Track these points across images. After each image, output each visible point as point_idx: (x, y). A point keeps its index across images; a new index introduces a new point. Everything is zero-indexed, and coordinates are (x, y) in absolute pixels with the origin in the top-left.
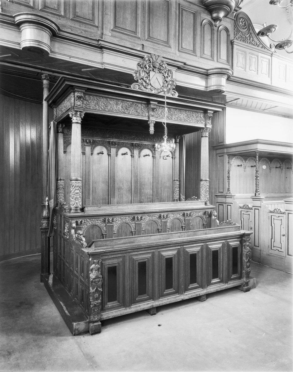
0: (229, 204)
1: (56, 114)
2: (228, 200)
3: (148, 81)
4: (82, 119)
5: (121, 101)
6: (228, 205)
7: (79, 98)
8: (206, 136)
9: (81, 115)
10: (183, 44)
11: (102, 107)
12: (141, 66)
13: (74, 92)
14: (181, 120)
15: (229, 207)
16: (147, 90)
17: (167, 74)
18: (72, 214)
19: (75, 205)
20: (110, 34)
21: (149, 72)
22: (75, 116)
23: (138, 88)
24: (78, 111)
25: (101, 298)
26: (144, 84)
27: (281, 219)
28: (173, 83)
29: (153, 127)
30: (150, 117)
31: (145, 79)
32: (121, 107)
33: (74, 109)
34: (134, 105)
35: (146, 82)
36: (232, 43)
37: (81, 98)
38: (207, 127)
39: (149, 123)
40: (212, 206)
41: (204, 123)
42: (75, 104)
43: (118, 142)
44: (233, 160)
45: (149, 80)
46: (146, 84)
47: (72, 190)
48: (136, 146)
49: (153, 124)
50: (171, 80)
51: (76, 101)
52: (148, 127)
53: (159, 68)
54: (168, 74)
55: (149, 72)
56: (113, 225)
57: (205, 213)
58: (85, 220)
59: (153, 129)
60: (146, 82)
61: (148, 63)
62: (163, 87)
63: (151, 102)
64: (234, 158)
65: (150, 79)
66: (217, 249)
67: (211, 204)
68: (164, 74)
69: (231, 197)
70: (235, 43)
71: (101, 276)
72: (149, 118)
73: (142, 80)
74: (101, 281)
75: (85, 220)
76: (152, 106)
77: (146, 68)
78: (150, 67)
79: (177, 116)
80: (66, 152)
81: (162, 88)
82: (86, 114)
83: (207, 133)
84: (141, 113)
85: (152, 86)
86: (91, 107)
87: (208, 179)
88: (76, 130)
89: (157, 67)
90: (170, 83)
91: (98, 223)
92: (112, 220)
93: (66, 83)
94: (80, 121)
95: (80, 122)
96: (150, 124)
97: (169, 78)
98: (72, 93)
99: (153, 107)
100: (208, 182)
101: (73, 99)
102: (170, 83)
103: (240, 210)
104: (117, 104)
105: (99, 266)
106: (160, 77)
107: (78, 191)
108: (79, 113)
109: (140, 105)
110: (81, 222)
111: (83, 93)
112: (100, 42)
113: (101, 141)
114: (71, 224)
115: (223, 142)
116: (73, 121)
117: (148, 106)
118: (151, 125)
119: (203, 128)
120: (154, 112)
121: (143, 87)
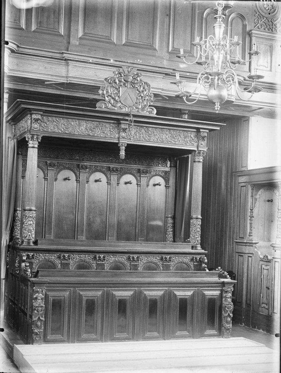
0: (250, 255)
1: (15, 132)
2: (246, 249)
3: (117, 98)
4: (39, 143)
5: (84, 121)
6: (249, 256)
7: (37, 120)
8: (199, 162)
9: (37, 138)
10: (175, 44)
11: (62, 130)
12: (109, 81)
13: (31, 114)
14: (162, 142)
15: (250, 259)
16: (116, 109)
17: (142, 88)
18: (25, 245)
19: (27, 237)
20: (78, 43)
21: (119, 87)
22: (31, 140)
23: (104, 107)
24: (34, 135)
25: (43, 328)
26: (112, 101)
27: (268, 269)
28: (150, 98)
29: (124, 151)
30: (120, 139)
31: (113, 96)
32: (84, 128)
33: (30, 132)
34: (101, 125)
35: (114, 99)
36: (250, 34)
37: (38, 120)
38: (200, 149)
39: (119, 145)
40: (203, 251)
41: (196, 144)
42: (31, 127)
43: (90, 165)
44: (260, 193)
45: (119, 96)
46: (114, 102)
47: (24, 221)
48: (114, 171)
49: (124, 147)
50: (147, 94)
51: (32, 124)
52: (119, 150)
53: (133, 81)
54: (143, 88)
55: (119, 87)
56: (69, 262)
57: (192, 260)
58: (38, 254)
59: (124, 153)
60: (114, 99)
61: (118, 78)
62: (137, 104)
63: (121, 122)
64: (261, 190)
65: (120, 96)
66: (186, 297)
67: (203, 249)
68: (139, 88)
69: (251, 244)
70: (253, 35)
71: (44, 306)
72: (119, 141)
73: (110, 98)
74: (44, 310)
75: (38, 254)
76: (123, 126)
77: (116, 83)
78: (120, 81)
79: (157, 137)
80: (25, 177)
81: (136, 104)
82: (43, 138)
83: (201, 157)
84: (109, 135)
85: (122, 104)
86: (50, 130)
87: (200, 217)
88: (33, 154)
89: (130, 80)
90: (146, 99)
91: (52, 259)
92: (69, 256)
93: (23, 106)
94: (37, 145)
95: (36, 146)
96: (121, 147)
97: (145, 93)
98: (29, 115)
99: (124, 127)
100: (200, 220)
101: (29, 121)
102: (146, 99)
103: (261, 263)
104: (80, 125)
105: (43, 297)
106: (133, 95)
107: (31, 222)
108: (35, 137)
109: (107, 125)
110: (33, 255)
111: (40, 115)
112: (65, 55)
113: (69, 163)
114: (22, 257)
115: (246, 167)
116: (30, 145)
117: (119, 126)
118: (121, 149)
119: (195, 151)
120: (126, 132)
121: (110, 105)
